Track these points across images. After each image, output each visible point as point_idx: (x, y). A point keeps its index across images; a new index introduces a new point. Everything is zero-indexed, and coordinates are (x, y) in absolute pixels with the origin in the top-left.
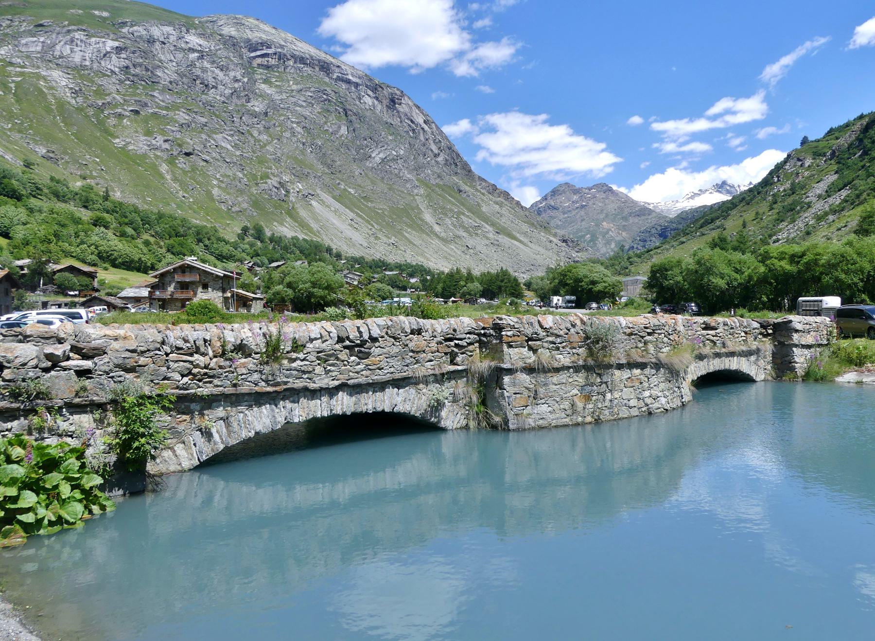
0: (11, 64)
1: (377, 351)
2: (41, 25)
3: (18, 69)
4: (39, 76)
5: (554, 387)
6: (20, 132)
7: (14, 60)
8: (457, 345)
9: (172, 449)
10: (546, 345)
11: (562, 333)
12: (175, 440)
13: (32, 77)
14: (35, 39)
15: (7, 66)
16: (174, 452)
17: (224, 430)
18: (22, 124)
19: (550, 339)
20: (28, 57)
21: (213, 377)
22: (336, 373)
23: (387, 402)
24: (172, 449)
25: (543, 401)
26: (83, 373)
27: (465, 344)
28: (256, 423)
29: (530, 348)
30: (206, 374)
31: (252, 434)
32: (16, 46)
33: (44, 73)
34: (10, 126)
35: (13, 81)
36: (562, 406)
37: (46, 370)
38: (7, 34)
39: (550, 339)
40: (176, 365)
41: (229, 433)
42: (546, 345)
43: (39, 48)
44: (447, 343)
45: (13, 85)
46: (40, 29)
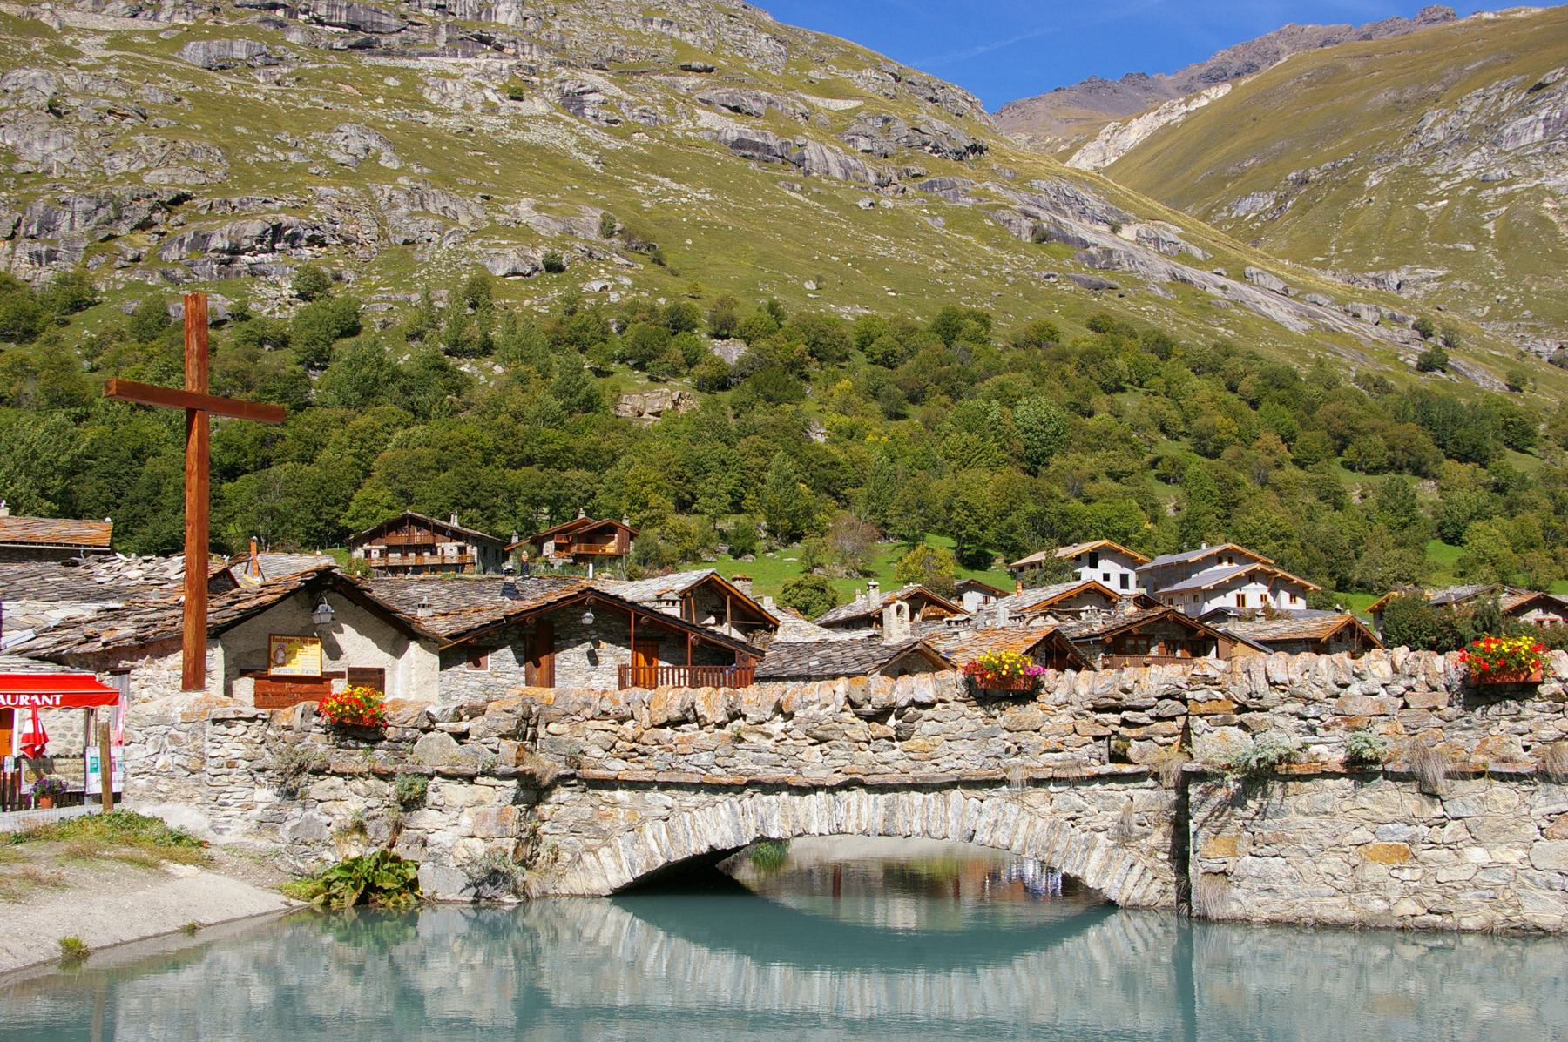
0: (1486, 182)
1: (928, 727)
2: (1541, 86)
3: (1501, 190)
4: (1539, 193)
5: (1300, 818)
6: (1506, 317)
7: (1492, 175)
8: (1125, 723)
9: (595, 853)
10: (1281, 721)
11: (1319, 693)
12: (599, 842)
13: (1528, 199)
14: (1530, 118)
15: (1480, 190)
16: (598, 858)
17: (664, 836)
18: (1511, 297)
19: (1291, 707)
20: (1518, 159)
21: (644, 754)
22: (842, 762)
23: (953, 823)
24: (595, 853)
25: (1272, 849)
26: (461, 737)
27: (1146, 719)
28: (710, 831)
29: (1243, 726)
30: (634, 750)
31: (704, 849)
32: (1495, 144)
33: (1550, 184)
34: (1487, 309)
35: (1492, 217)
36: (1322, 868)
37: (426, 731)
38: (1478, 126)
39: (1291, 707)
40: (596, 735)
41: (673, 839)
42: (1281, 721)
43: (1539, 135)
44: (1099, 716)
45: (1490, 226)
46: (1539, 93)
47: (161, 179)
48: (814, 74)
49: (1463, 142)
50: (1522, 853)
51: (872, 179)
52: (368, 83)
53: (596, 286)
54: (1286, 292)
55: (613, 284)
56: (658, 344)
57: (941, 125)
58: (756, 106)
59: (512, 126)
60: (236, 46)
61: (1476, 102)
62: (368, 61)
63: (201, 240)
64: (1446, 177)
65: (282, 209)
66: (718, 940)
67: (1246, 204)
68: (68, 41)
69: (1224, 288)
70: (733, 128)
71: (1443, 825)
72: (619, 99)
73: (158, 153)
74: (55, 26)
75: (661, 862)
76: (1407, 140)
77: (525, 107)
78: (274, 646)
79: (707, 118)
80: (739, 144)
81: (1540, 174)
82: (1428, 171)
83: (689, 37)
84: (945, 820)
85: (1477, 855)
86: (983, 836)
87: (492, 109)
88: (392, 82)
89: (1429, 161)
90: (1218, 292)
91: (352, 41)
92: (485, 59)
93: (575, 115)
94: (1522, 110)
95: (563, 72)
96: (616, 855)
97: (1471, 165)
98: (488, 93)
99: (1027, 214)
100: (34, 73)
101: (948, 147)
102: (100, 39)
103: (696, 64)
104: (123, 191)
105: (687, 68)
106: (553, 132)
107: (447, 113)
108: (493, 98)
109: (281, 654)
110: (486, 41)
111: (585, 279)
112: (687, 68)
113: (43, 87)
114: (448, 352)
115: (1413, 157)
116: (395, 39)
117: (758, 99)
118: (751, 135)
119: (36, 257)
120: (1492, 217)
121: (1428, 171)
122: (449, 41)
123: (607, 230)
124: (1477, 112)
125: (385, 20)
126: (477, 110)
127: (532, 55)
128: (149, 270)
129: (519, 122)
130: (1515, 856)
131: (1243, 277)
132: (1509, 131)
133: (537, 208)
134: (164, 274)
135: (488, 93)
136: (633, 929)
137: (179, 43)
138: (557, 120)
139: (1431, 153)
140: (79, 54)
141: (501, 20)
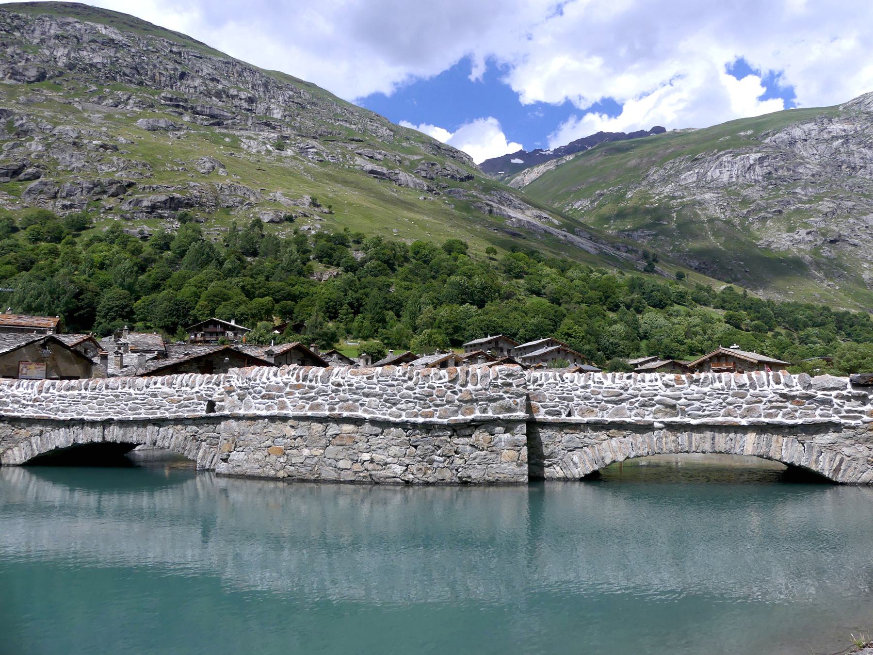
0: (674, 198)
2: (696, 159)
20: (686, 188)
45: (674, 215)
47: (123, 176)
48: (404, 144)
49: (665, 181)
50: (322, 451)
51: (426, 188)
52: (217, 140)
53: (306, 228)
54: (591, 239)
55: (311, 227)
56: (332, 250)
57: (454, 167)
58: (379, 157)
59: (277, 160)
60: (160, 121)
61: (671, 165)
62: (217, 130)
63: (138, 202)
64: (658, 195)
65: (174, 191)
66: (55, 481)
67: (579, 203)
68: (86, 115)
69: (565, 236)
70: (369, 166)
71: (295, 439)
72: (323, 151)
73: (122, 165)
74: (80, 108)
75: (37, 453)
76: (644, 179)
77: (283, 153)
78: (21, 366)
79: (359, 160)
80: (372, 172)
81: (695, 195)
82: (650, 192)
83: (353, 126)
84: (146, 436)
85: (306, 452)
86: (159, 443)
87: (268, 152)
88: (227, 140)
89: (652, 188)
90: (563, 238)
91: (212, 122)
92: (266, 133)
93: (304, 157)
94: (689, 169)
95: (300, 139)
96: (20, 451)
97: (668, 190)
98: (268, 146)
99: (487, 204)
100: (68, 128)
101: (458, 176)
102: (100, 115)
103: (356, 138)
104: (105, 180)
105: (353, 140)
106: (293, 164)
107: (250, 154)
108: (270, 148)
109: (25, 369)
110: (267, 124)
111: (302, 225)
112: (353, 140)
113: (71, 133)
114: (243, 253)
115: (645, 186)
116: (230, 122)
117: (380, 154)
118: (378, 169)
119: (65, 207)
120: (675, 211)
121: (650, 192)
122: (253, 123)
123: (314, 203)
124: (671, 169)
125: (226, 114)
126: (263, 153)
127: (288, 132)
128: (115, 214)
129: (280, 159)
130: (319, 452)
131: (573, 233)
132: (683, 177)
133: (285, 195)
134: (122, 216)
135: (268, 146)
136: (24, 477)
137: (135, 119)
138: (296, 159)
139: (652, 185)
140: (91, 121)
141: (275, 116)
